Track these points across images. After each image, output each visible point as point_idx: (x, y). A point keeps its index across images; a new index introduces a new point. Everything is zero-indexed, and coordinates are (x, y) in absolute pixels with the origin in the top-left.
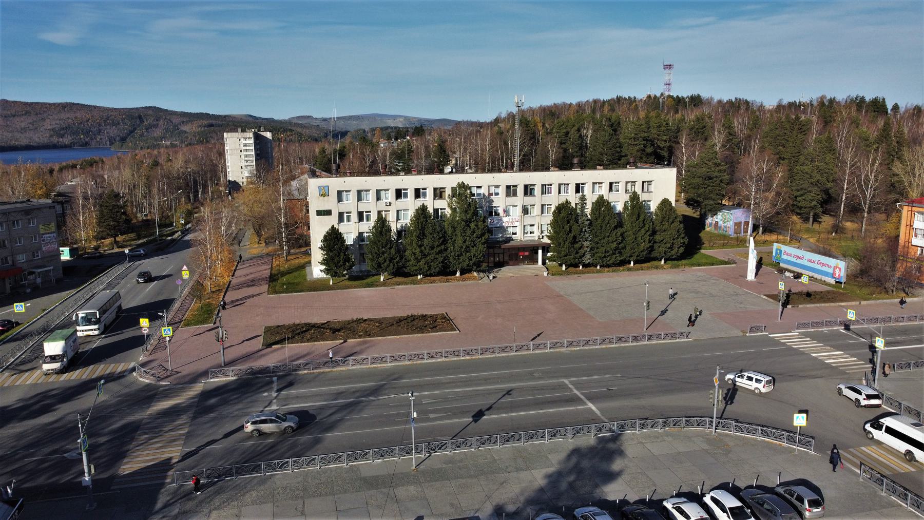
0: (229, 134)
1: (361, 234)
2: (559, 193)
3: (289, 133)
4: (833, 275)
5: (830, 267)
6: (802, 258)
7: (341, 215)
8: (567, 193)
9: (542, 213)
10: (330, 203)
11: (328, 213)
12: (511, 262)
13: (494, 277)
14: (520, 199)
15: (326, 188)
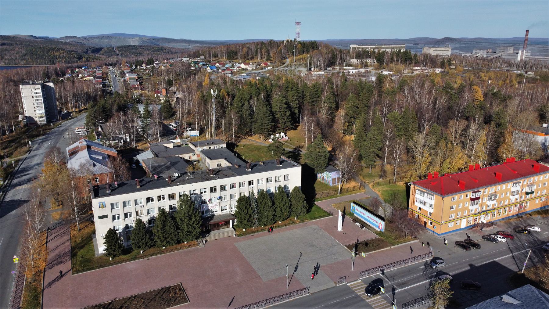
0: (24, 86)
1: (127, 225)
2: (240, 186)
3: (61, 52)
4: (379, 227)
5: (377, 223)
6: (365, 214)
7: (114, 217)
8: (244, 186)
9: (231, 198)
10: (107, 211)
11: (106, 216)
12: (215, 229)
13: (206, 241)
14: (218, 193)
15: (104, 204)
